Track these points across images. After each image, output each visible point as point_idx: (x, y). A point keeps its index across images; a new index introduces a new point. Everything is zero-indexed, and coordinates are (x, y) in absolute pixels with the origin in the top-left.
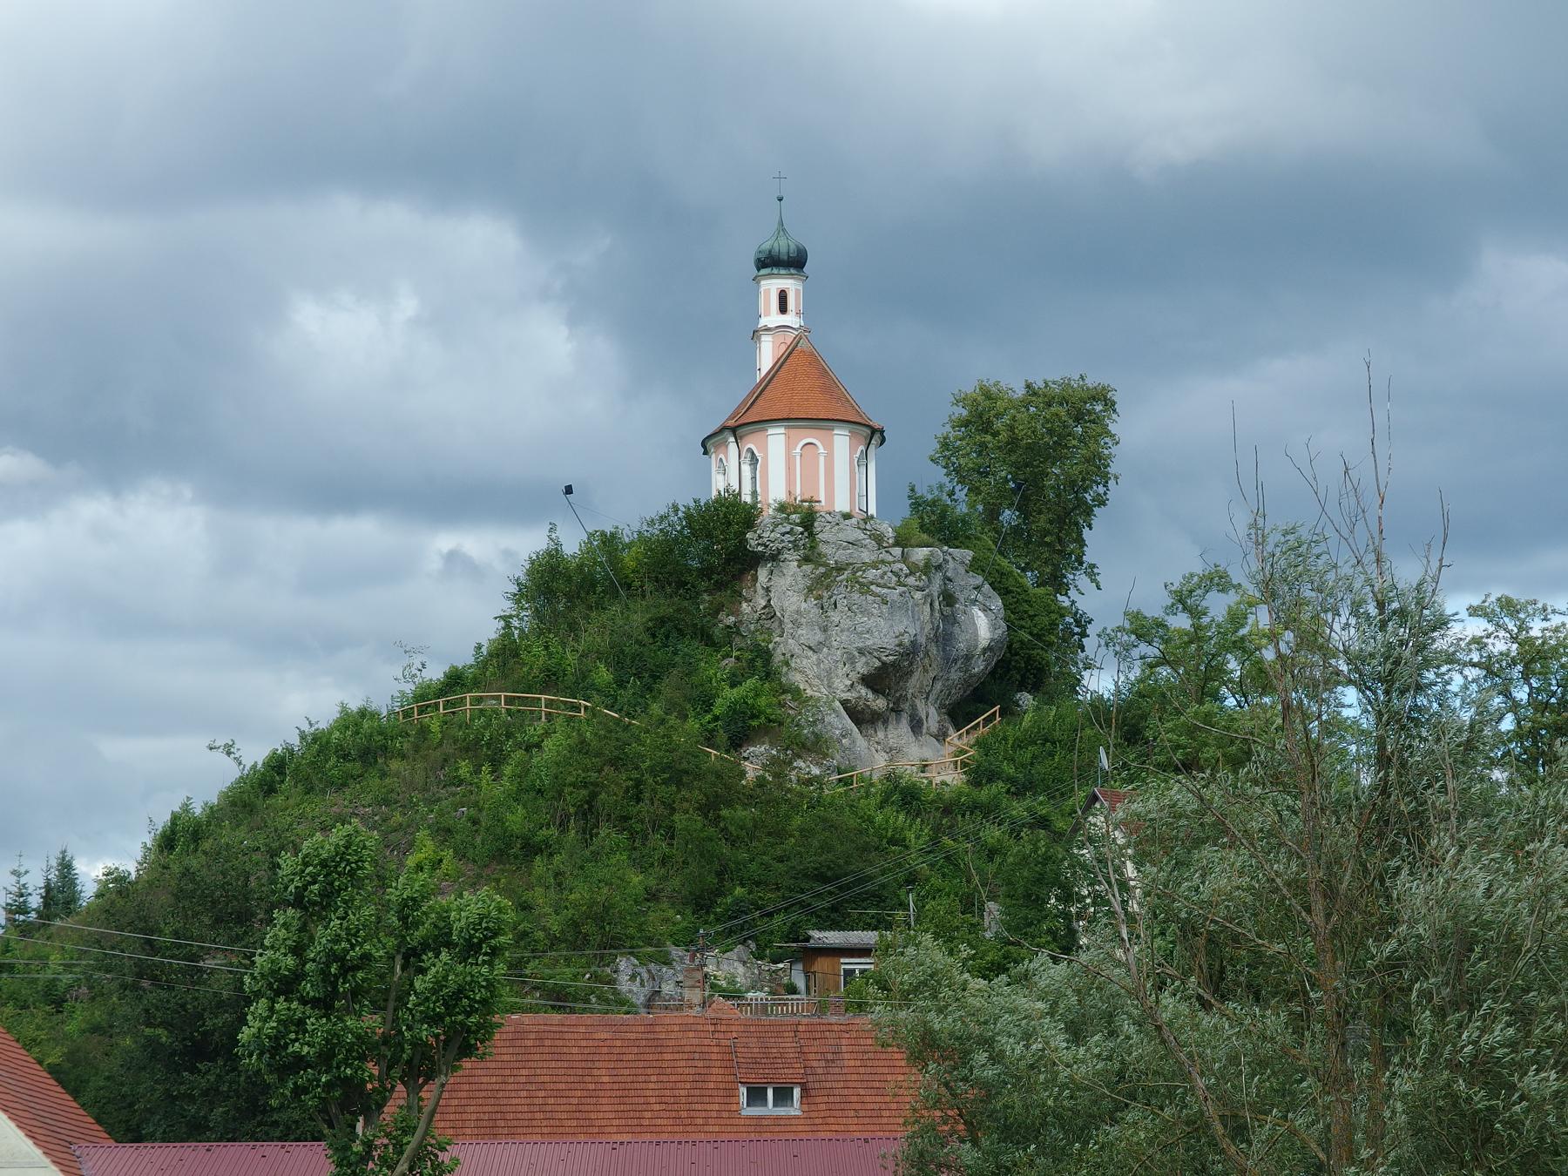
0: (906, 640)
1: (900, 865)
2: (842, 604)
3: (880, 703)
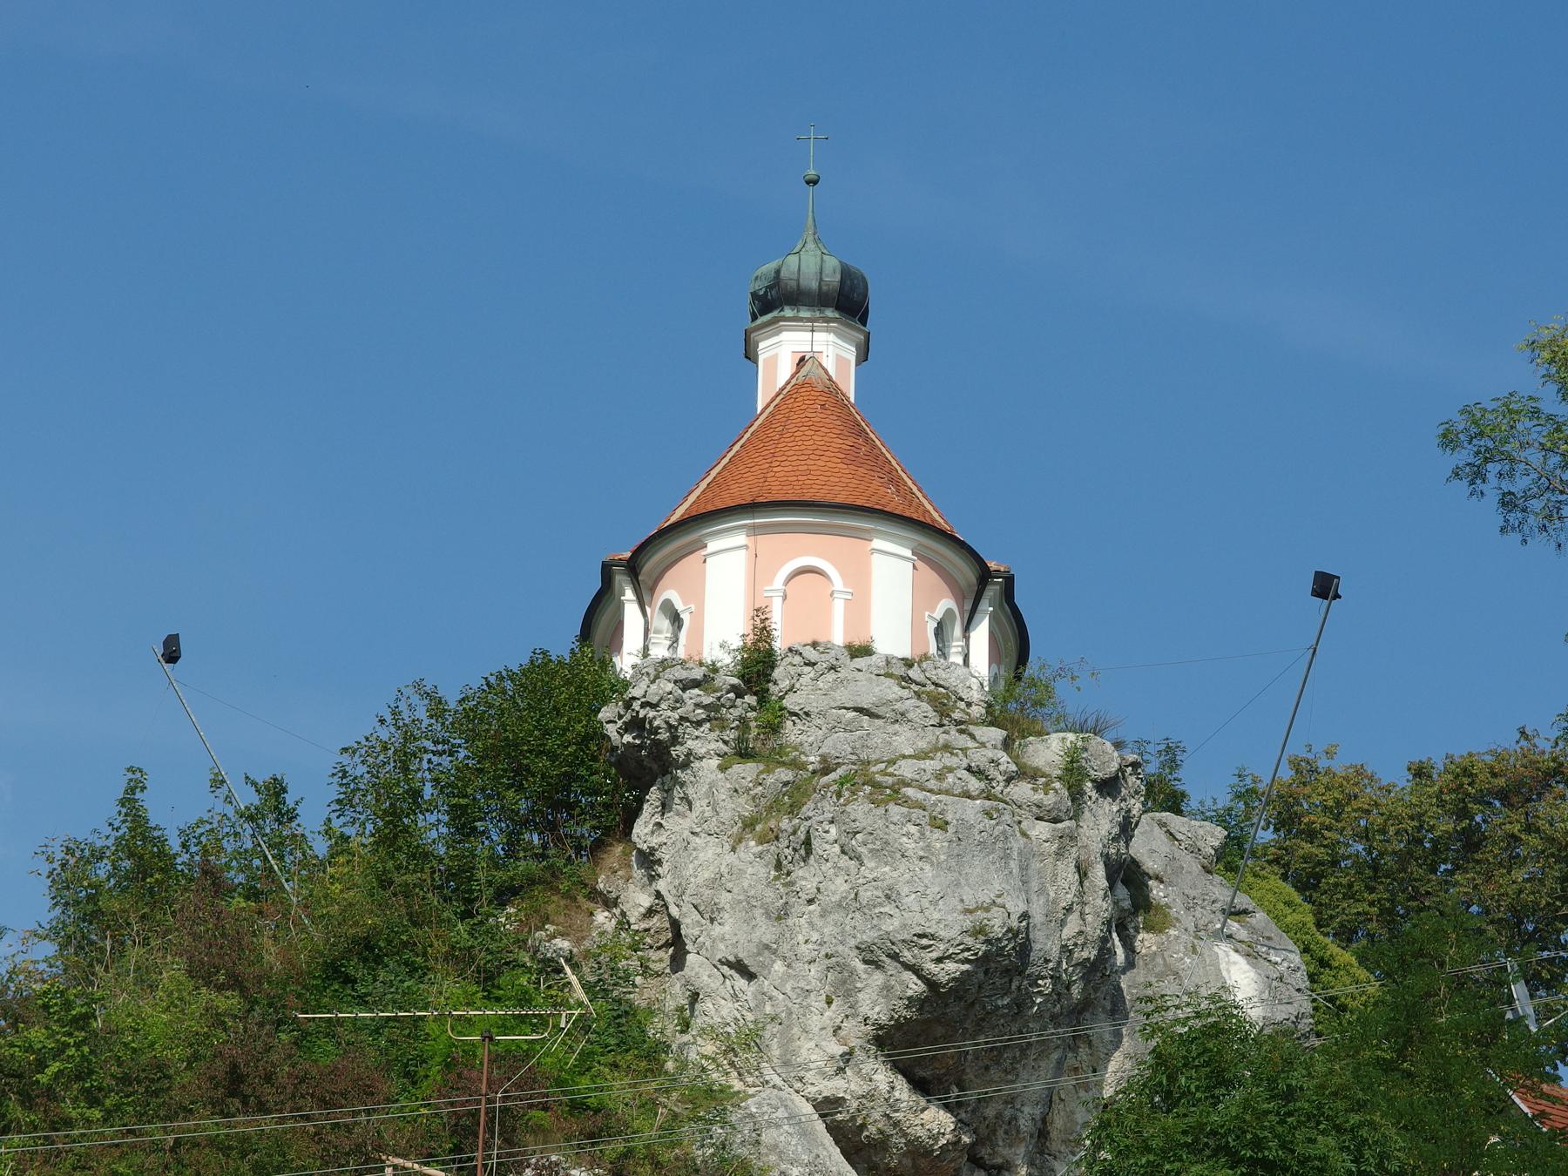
0: (997, 929)
1: (385, 882)
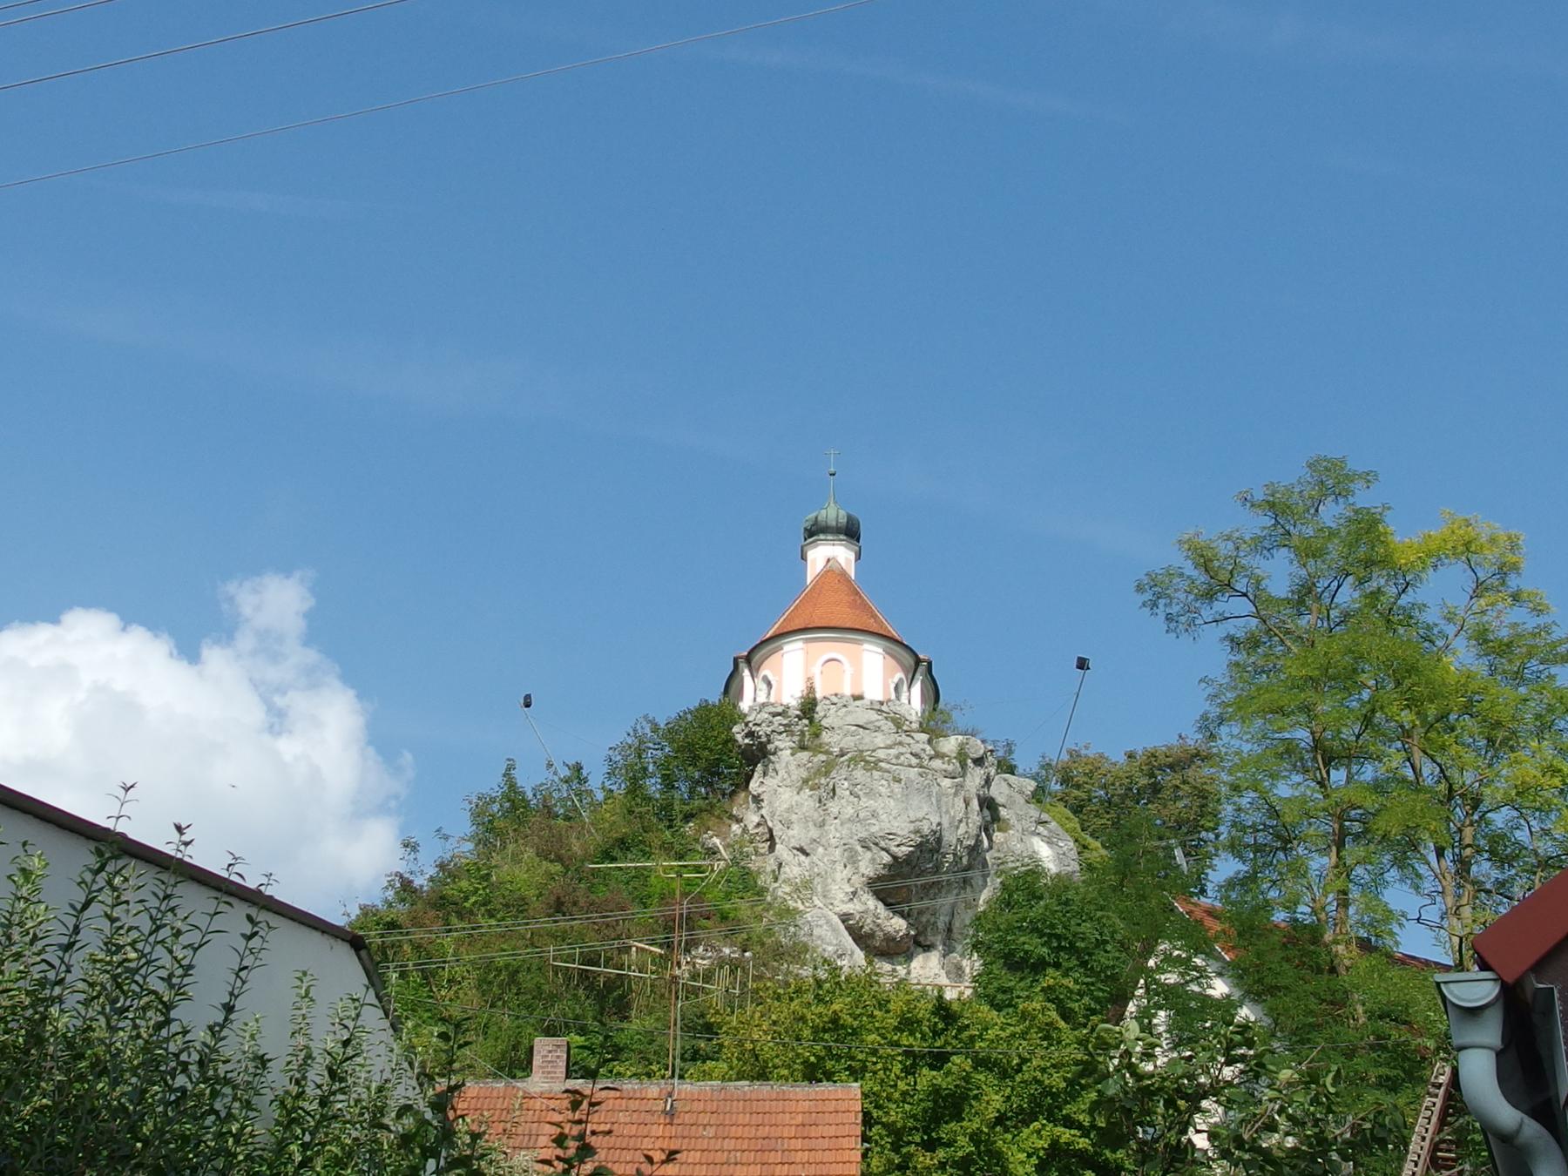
2: (843, 788)
3: (898, 925)
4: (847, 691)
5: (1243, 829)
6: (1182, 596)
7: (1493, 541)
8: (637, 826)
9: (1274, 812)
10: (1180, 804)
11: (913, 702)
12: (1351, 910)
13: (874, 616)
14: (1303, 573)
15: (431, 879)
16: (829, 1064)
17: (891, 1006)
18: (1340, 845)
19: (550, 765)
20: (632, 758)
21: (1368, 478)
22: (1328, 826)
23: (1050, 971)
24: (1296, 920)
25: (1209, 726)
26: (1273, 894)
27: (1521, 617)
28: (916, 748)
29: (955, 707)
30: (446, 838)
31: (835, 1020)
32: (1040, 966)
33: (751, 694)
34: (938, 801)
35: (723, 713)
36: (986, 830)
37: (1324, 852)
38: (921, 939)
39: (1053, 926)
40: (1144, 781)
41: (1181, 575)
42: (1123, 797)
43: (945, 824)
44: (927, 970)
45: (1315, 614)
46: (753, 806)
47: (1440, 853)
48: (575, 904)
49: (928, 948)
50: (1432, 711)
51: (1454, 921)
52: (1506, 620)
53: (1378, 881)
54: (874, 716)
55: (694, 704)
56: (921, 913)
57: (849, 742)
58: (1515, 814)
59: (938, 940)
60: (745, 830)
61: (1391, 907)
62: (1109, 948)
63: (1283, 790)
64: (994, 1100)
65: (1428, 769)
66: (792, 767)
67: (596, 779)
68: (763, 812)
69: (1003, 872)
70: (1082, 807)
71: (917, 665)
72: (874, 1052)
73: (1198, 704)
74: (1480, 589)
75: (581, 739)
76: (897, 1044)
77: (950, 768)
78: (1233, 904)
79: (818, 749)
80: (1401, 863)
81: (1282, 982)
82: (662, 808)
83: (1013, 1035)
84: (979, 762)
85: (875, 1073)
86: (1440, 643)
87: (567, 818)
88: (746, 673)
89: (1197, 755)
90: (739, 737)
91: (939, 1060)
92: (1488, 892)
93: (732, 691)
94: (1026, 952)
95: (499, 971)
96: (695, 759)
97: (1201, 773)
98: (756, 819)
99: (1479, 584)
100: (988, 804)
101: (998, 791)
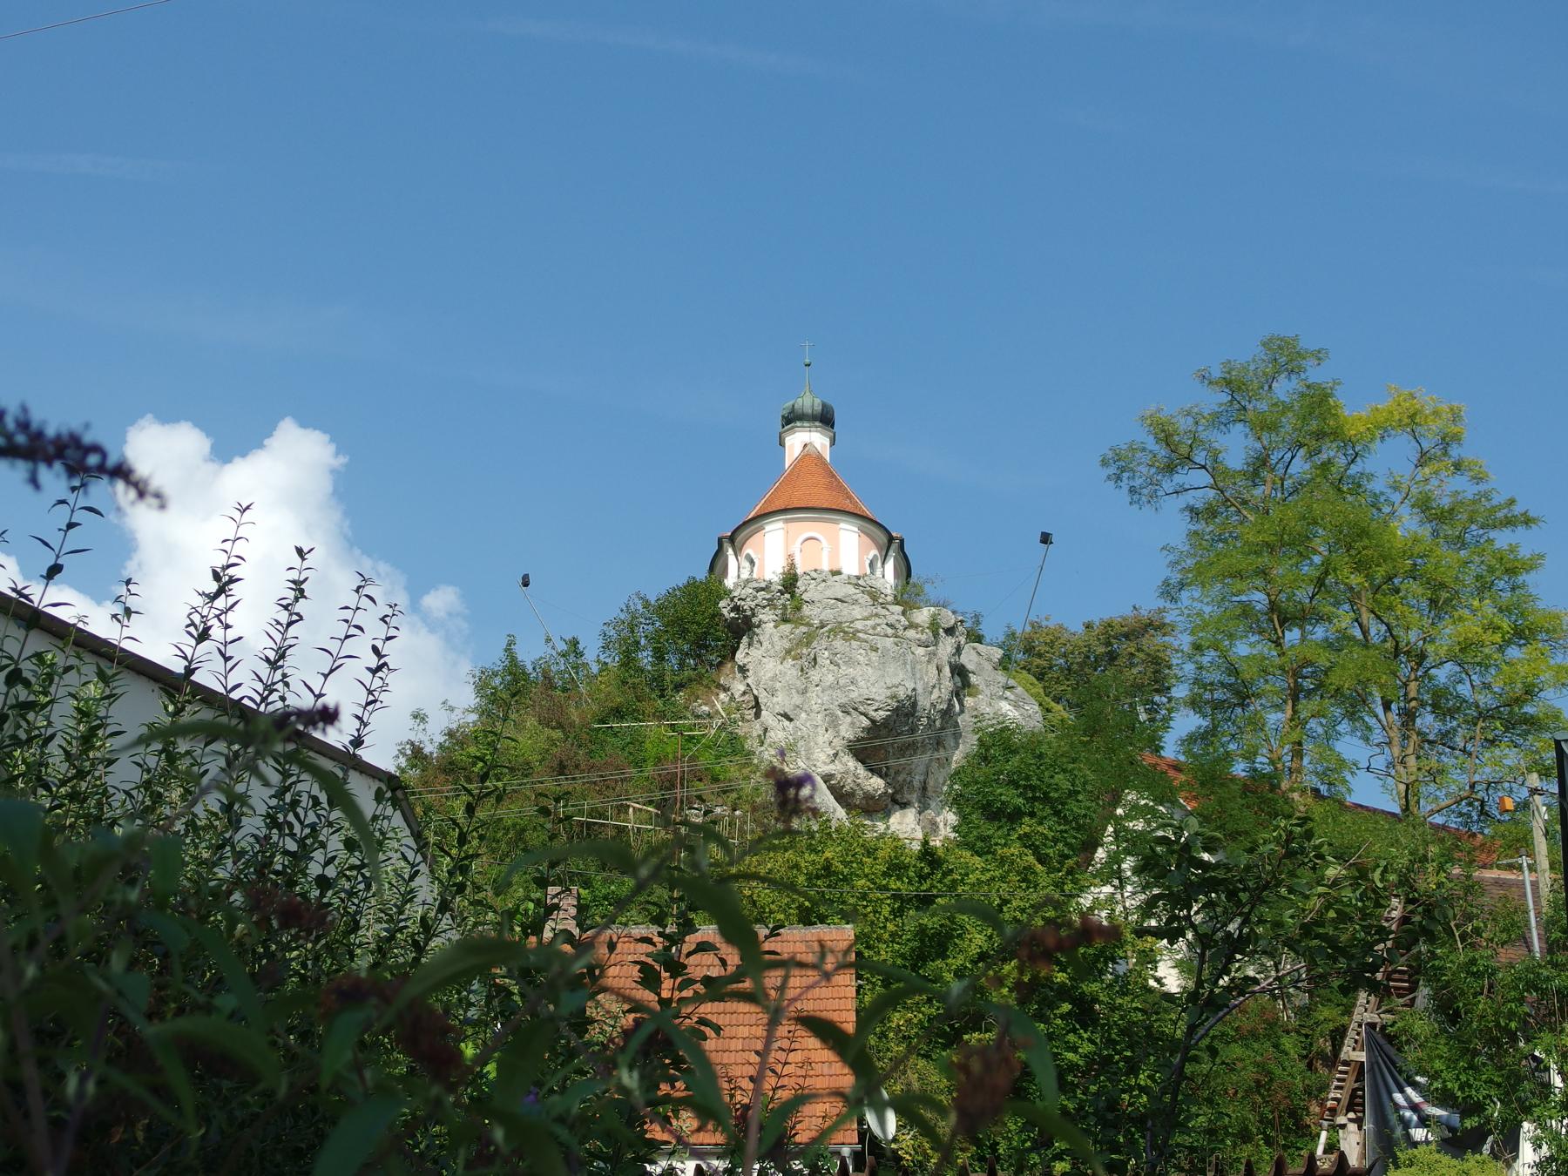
3: (876, 784)
4: (826, 567)
5: (1204, 686)
6: (1144, 470)
7: (1436, 413)
8: (631, 696)
9: (1233, 670)
10: (1135, 671)
11: (888, 575)
12: (1306, 761)
13: (849, 497)
14: (1258, 445)
15: (441, 746)
16: (822, 910)
17: (880, 854)
18: (1295, 700)
19: (548, 640)
20: (625, 633)
21: (1319, 356)
22: (1280, 683)
23: (1026, 819)
24: (1255, 770)
25: (1170, 591)
26: (1232, 747)
27: (1461, 485)
28: (891, 619)
29: (926, 581)
30: (452, 709)
31: (827, 867)
32: (1015, 816)
33: (735, 572)
34: (913, 668)
35: (706, 591)
36: (957, 695)
37: (1278, 707)
38: (898, 797)
39: (1028, 778)
40: (1101, 650)
41: (1144, 449)
42: (1082, 665)
43: (920, 690)
44: (905, 825)
45: (1269, 485)
46: (739, 675)
47: (1387, 707)
48: (577, 766)
49: (904, 805)
50: (1380, 573)
51: (1400, 768)
52: (1448, 488)
53: (1331, 734)
54: (851, 590)
55: (682, 581)
56: (897, 773)
57: (827, 615)
58: (1458, 669)
59: (914, 797)
60: (732, 698)
61: (1345, 756)
62: (1080, 797)
63: (1242, 649)
64: (977, 939)
65: (1376, 630)
66: (776, 639)
67: (592, 652)
68: (749, 681)
69: (980, 729)
70: (1043, 674)
71: (891, 543)
72: (864, 897)
73: (1162, 571)
74: (1424, 459)
75: (581, 612)
76: (886, 888)
77: (924, 637)
78: (1195, 756)
79: (799, 622)
80: (1352, 716)
81: (1243, 827)
82: (654, 679)
83: (993, 879)
84: (950, 631)
85: (865, 915)
86: (1387, 509)
87: (565, 690)
88: (730, 552)
89: (1151, 624)
90: (725, 612)
91: (925, 901)
92: (1430, 742)
93: (718, 569)
94: (1003, 803)
95: (507, 830)
96: (683, 632)
97: (1153, 642)
98: (742, 688)
99: (1423, 454)
100: (959, 671)
101: (968, 659)
